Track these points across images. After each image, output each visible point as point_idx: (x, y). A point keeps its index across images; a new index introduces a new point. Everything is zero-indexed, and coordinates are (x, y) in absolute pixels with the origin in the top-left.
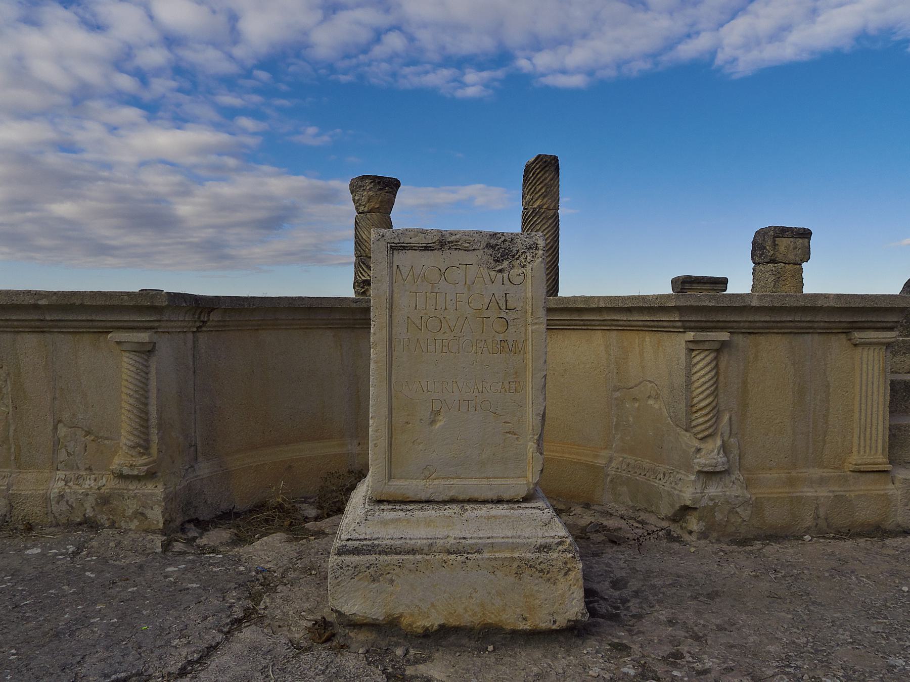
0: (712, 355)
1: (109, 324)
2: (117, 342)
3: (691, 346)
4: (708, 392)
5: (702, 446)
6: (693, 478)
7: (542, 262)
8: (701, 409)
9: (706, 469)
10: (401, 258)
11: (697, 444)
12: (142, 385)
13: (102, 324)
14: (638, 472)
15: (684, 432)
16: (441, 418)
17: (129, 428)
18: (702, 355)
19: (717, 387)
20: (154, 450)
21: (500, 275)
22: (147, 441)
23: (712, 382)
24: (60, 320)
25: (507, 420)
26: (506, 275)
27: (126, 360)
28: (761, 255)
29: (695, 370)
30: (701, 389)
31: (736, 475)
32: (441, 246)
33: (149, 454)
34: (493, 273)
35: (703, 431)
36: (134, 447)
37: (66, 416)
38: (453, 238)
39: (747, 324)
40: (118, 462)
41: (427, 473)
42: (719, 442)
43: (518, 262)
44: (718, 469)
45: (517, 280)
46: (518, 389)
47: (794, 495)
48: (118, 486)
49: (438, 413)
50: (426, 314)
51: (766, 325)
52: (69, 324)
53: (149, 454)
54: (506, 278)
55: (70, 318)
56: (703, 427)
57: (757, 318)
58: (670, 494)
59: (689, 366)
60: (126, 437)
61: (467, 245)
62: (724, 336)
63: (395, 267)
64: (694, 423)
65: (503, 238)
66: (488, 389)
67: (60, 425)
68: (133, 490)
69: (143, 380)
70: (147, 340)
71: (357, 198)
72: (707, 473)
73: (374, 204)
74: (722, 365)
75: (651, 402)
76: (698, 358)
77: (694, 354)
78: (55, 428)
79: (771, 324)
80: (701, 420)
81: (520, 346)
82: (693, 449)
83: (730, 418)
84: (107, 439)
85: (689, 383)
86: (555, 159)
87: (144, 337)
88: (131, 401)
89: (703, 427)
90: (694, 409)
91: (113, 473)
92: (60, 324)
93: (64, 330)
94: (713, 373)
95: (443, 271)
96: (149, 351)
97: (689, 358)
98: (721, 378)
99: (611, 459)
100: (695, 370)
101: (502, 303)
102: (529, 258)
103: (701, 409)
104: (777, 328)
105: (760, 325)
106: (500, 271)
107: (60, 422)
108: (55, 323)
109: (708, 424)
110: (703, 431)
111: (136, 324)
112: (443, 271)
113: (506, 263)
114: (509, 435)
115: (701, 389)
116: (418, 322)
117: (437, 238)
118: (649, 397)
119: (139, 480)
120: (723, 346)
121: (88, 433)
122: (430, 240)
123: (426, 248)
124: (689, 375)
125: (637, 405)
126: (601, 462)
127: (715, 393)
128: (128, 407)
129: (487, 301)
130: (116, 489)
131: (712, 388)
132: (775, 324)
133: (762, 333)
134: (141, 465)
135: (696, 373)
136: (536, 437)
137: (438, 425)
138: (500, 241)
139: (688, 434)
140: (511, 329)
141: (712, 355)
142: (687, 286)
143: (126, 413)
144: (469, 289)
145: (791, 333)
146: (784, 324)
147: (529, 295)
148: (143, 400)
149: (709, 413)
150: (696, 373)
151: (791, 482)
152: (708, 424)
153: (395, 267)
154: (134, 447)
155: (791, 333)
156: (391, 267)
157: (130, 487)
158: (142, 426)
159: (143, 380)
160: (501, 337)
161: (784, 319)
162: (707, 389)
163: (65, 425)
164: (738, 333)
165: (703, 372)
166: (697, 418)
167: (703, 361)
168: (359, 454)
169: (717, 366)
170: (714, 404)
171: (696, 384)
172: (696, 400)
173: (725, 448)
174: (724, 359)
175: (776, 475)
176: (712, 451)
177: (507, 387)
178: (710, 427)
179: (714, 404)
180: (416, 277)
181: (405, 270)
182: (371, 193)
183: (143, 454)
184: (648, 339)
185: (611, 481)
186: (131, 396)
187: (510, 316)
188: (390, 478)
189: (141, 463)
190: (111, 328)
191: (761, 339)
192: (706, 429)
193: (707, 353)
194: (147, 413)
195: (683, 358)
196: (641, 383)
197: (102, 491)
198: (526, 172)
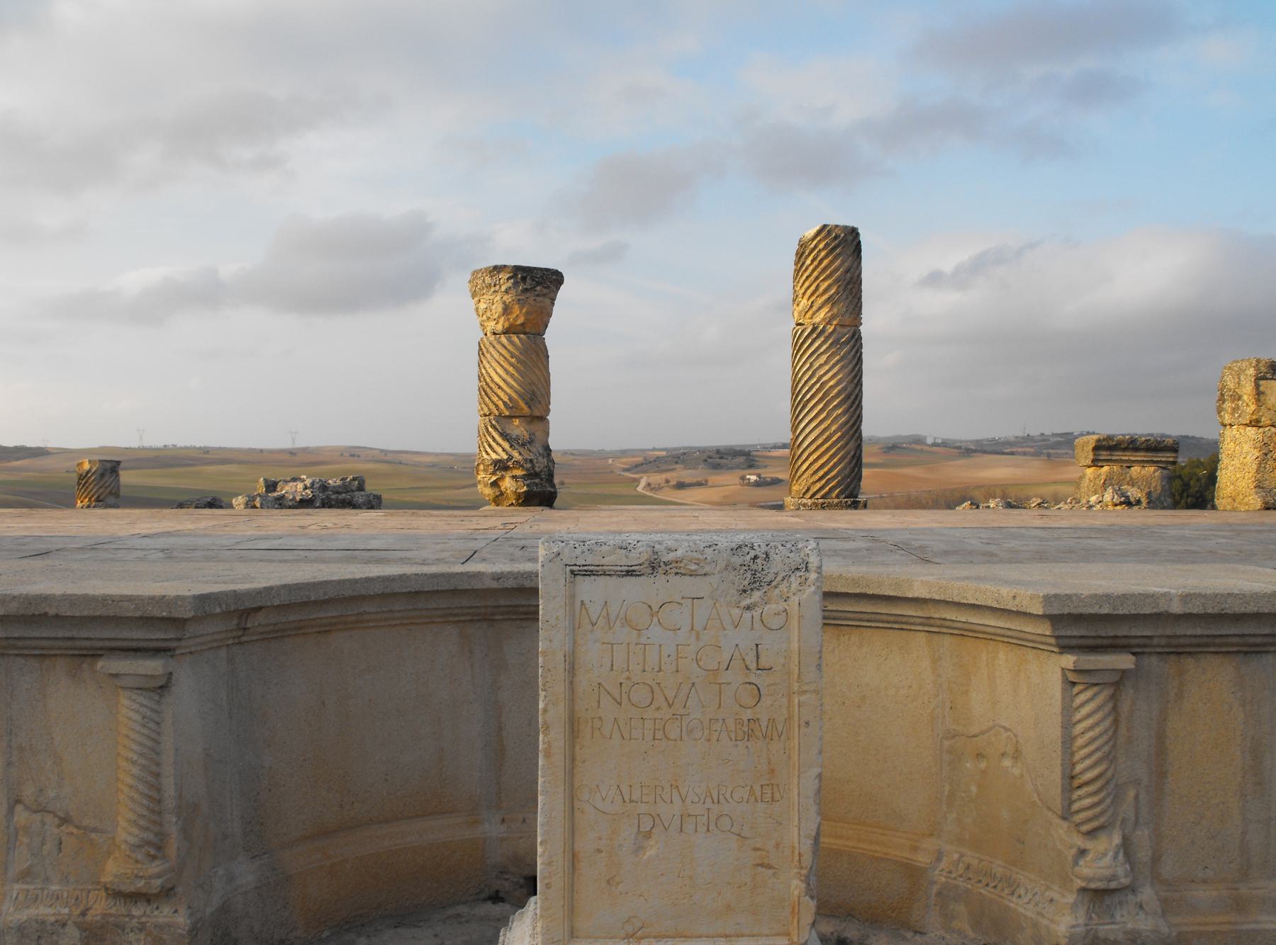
0: (1107, 692)
1: (100, 644)
2: (112, 675)
3: (1072, 677)
4: (1099, 754)
5: (1089, 845)
6: (1071, 898)
7: (815, 593)
8: (1087, 783)
9: (1093, 886)
10: (589, 589)
11: (1080, 842)
12: (149, 743)
13: (87, 644)
14: (984, 881)
15: (1058, 821)
16: (652, 843)
17: (132, 816)
18: (1089, 694)
19: (1114, 746)
20: (174, 846)
21: (747, 615)
22: (162, 835)
23: (1105, 738)
24: (19, 639)
25: (757, 846)
26: (756, 613)
27: (125, 702)
28: (1234, 410)
29: (1078, 716)
30: (1086, 751)
31: (1147, 894)
32: (653, 568)
33: (164, 857)
34: (736, 612)
35: (1090, 820)
36: (139, 847)
37: (29, 791)
38: (671, 556)
39: (1163, 641)
40: (113, 870)
41: (629, 929)
42: (1117, 840)
43: (777, 591)
44: (1113, 885)
45: (776, 622)
46: (777, 796)
47: (1246, 927)
48: (113, 911)
49: (648, 835)
50: (628, 678)
51: (1194, 641)
52: (34, 643)
53: (164, 857)
54: (757, 619)
55: (37, 634)
56: (1089, 813)
57: (1180, 631)
58: (1035, 925)
59: (1068, 710)
60: (126, 831)
61: (694, 567)
62: (1125, 661)
63: (578, 604)
64: (1076, 806)
65: (752, 554)
66: (728, 796)
67: (19, 808)
68: (139, 917)
69: (153, 735)
70: (160, 671)
71: (482, 306)
72: (1096, 891)
73: (518, 315)
74: (1125, 707)
75: (1007, 763)
76: (1082, 698)
77: (1076, 689)
78: (11, 811)
79: (1204, 640)
80: (1087, 802)
81: (780, 729)
82: (1074, 851)
83: (1136, 797)
84: (95, 830)
85: (1068, 740)
86: (854, 232)
87: (153, 666)
88: (135, 770)
89: (1089, 813)
90: (1076, 783)
91: (107, 889)
92: (20, 643)
93: (26, 652)
94: (1107, 723)
95: (655, 608)
96: (161, 687)
97: (1067, 700)
98: (1123, 731)
99: (939, 856)
100: (1078, 716)
101: (751, 660)
102: (794, 586)
103: (1087, 783)
104: (1214, 645)
105: (1187, 641)
106: (748, 608)
107: (18, 801)
108: (11, 642)
109: (1098, 810)
110: (1090, 820)
111: (141, 644)
112: (655, 608)
113: (756, 595)
114: (760, 869)
115: (1086, 751)
116: (616, 693)
117: (644, 557)
118: (1003, 755)
119: (149, 901)
120: (1120, 680)
121: (65, 820)
122: (634, 559)
123: (629, 573)
124: (1067, 725)
125: (983, 765)
126: (922, 859)
127: (1110, 758)
128: (130, 781)
129: (727, 656)
130: (111, 915)
131: (1106, 748)
132: (1209, 640)
133: (1190, 653)
134: (151, 877)
135: (1079, 721)
136: (804, 872)
137: (651, 852)
138: (748, 558)
139: (1065, 825)
140: (766, 701)
141: (1107, 692)
142: (1104, 455)
143: (126, 790)
144: (698, 638)
145: (1238, 652)
146: (1224, 640)
147: (795, 645)
148: (153, 768)
149: (1095, 793)
150: (1079, 721)
151: (1240, 905)
152: (1098, 810)
153: (578, 604)
154: (139, 847)
155: (1238, 652)
156: (572, 604)
157: (135, 912)
158: (153, 811)
159: (153, 735)
160: (748, 714)
161: (1224, 632)
162: (1097, 749)
163: (27, 808)
164: (1150, 654)
165: (1090, 722)
166: (1080, 798)
167: (1089, 704)
168: (503, 839)
169: (1115, 708)
170: (1109, 774)
171: (1080, 742)
172: (1079, 768)
173: (1127, 847)
174: (1128, 696)
175: (1214, 893)
176: (1105, 855)
177: (758, 794)
178: (1102, 813)
179: (1109, 774)
180: (612, 618)
181: (595, 610)
182: (508, 298)
183: (154, 858)
184: (1002, 655)
185: (939, 894)
186: (134, 763)
187: (763, 680)
188: (573, 934)
189: (153, 873)
190: (101, 649)
191: (1189, 662)
192: (1095, 817)
193: (1096, 689)
194: (159, 790)
195: (1058, 694)
196: (990, 729)
197: (88, 918)
198: (800, 255)
